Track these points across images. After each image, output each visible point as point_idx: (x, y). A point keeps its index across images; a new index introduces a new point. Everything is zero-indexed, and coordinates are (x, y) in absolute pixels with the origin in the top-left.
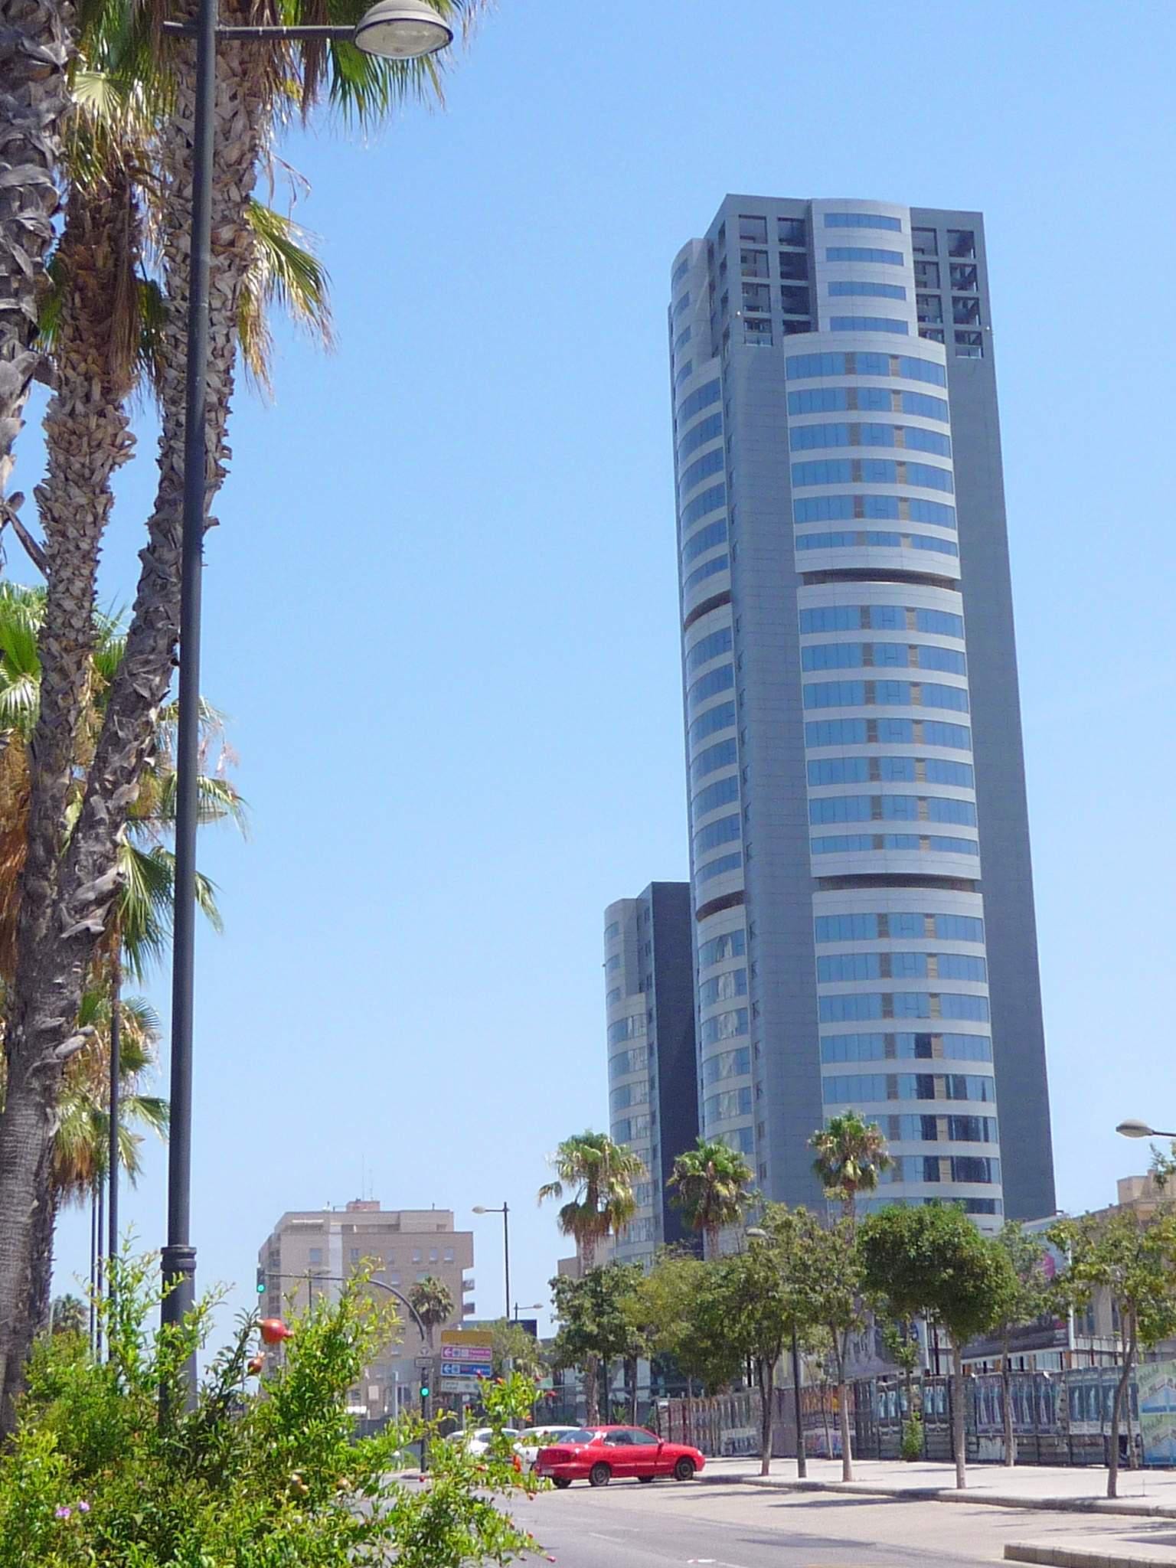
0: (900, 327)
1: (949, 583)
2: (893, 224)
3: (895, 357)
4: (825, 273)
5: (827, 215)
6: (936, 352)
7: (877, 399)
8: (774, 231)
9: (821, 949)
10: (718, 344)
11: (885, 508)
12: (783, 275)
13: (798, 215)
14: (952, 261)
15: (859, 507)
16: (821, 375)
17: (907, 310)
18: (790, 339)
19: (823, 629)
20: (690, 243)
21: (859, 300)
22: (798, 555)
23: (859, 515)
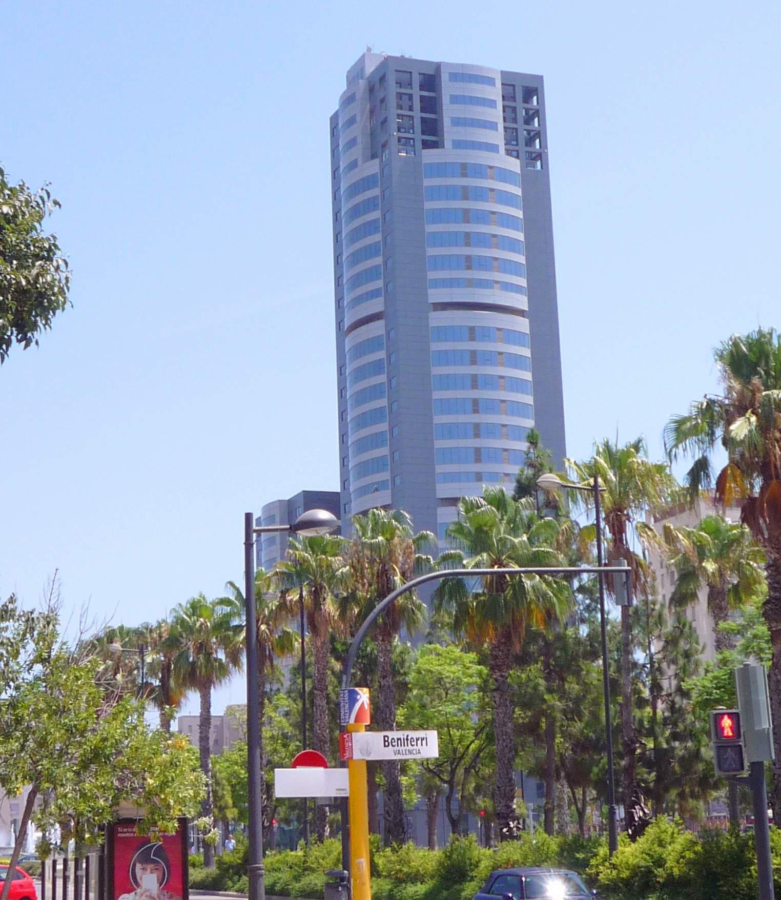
0: (493, 148)
1: (521, 313)
2: (490, 81)
3: (491, 167)
4: (449, 111)
5: (450, 74)
6: (514, 165)
7: (481, 194)
8: (416, 80)
9: (439, 444)
10: (376, 150)
11: (486, 264)
12: (423, 133)
13: (431, 72)
14: (524, 99)
15: (469, 263)
16: (455, 365)
17: (498, 137)
18: (426, 152)
19: (449, 412)
20: (362, 59)
21: (469, 130)
22: (431, 291)
23: (469, 268)
